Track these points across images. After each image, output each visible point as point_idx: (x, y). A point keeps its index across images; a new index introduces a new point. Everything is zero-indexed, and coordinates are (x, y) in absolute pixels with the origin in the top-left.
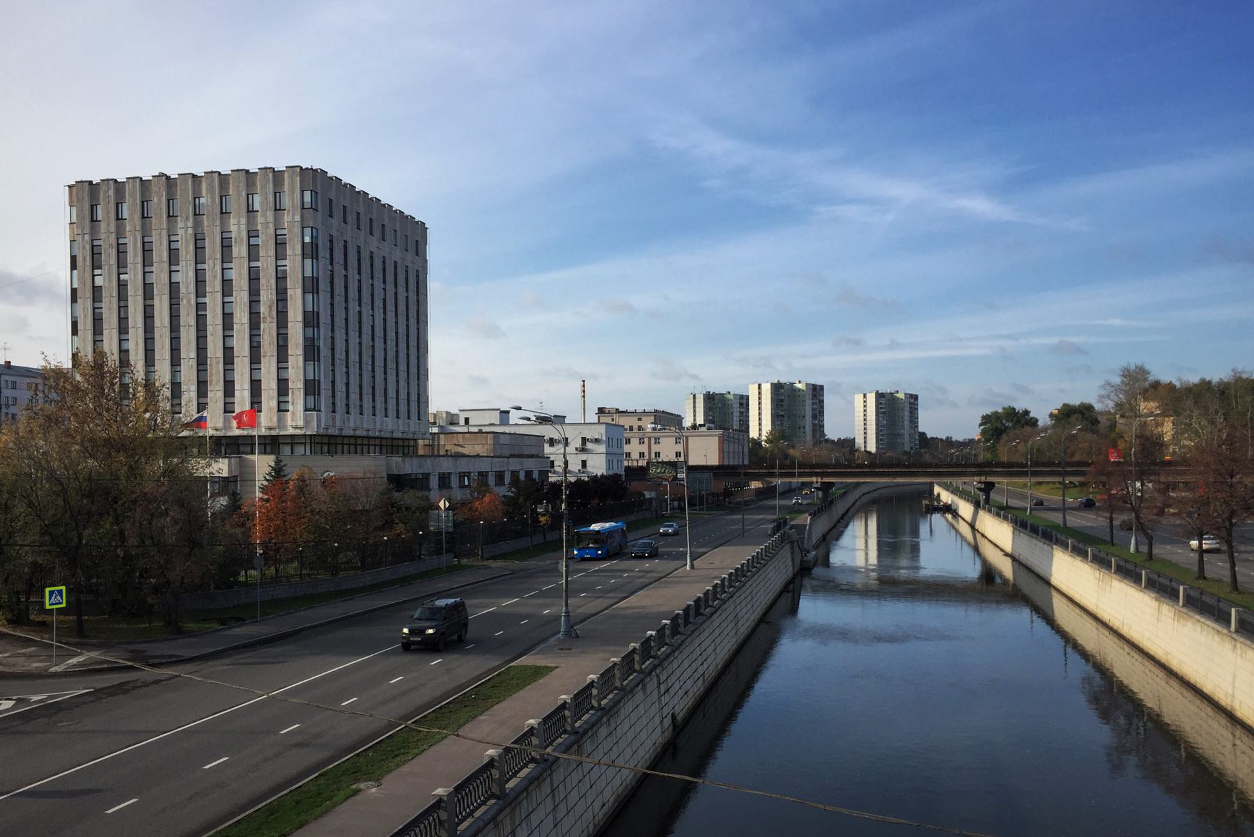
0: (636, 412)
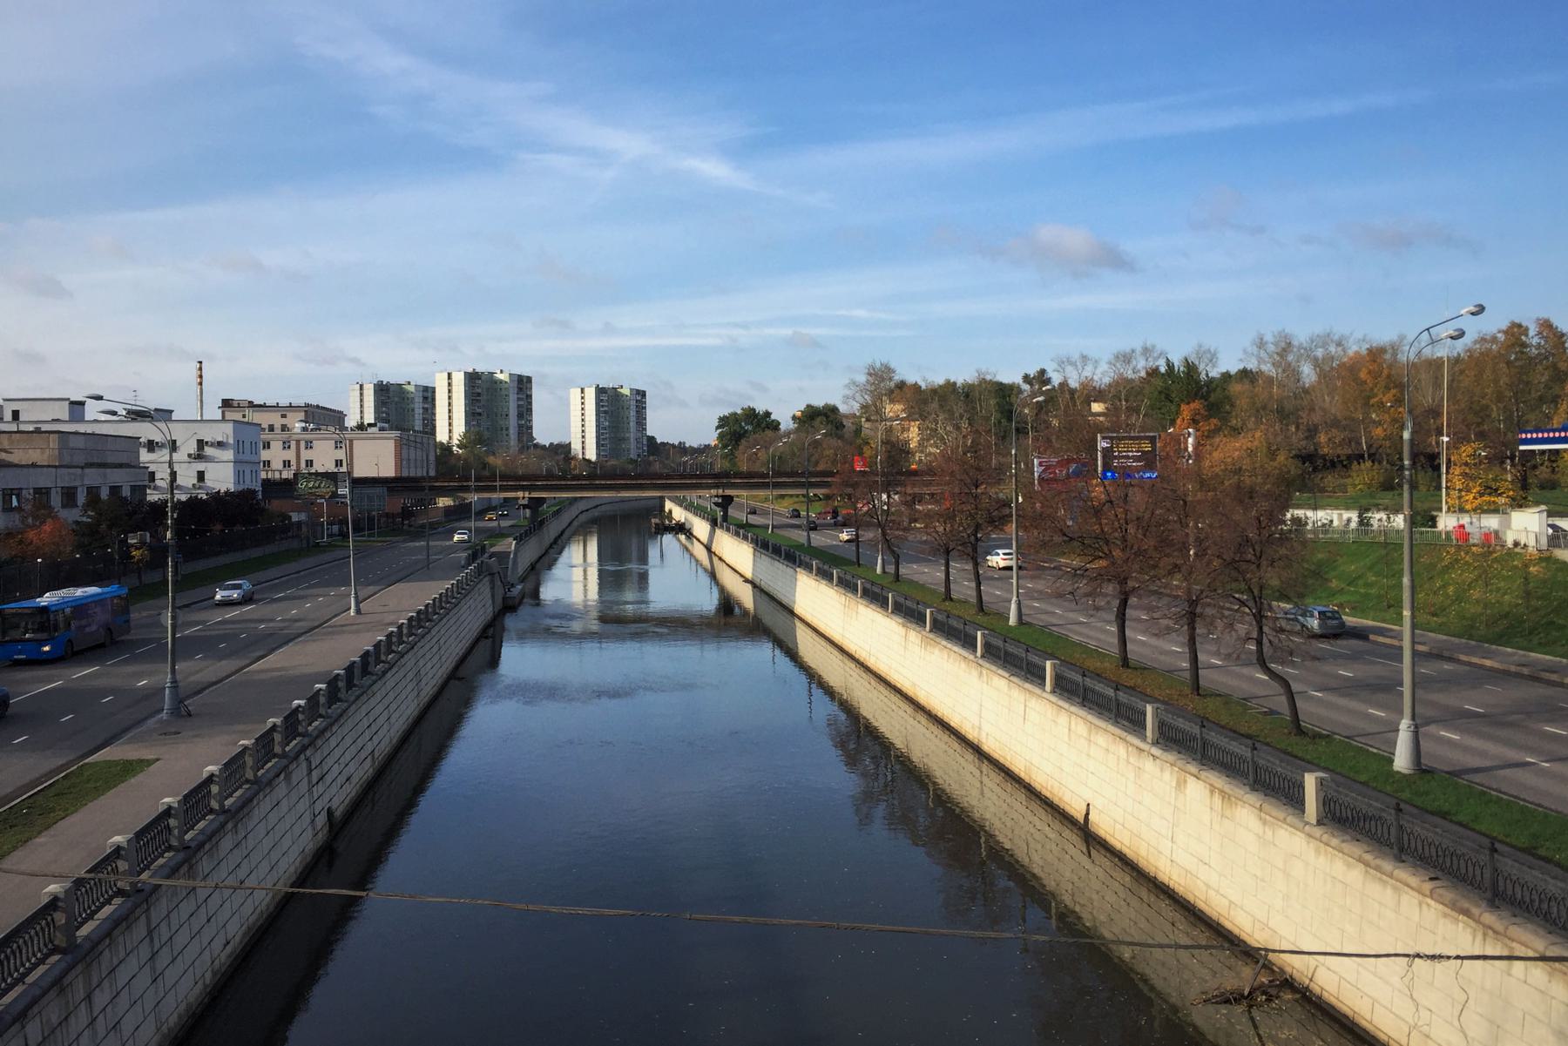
0: (291, 407)
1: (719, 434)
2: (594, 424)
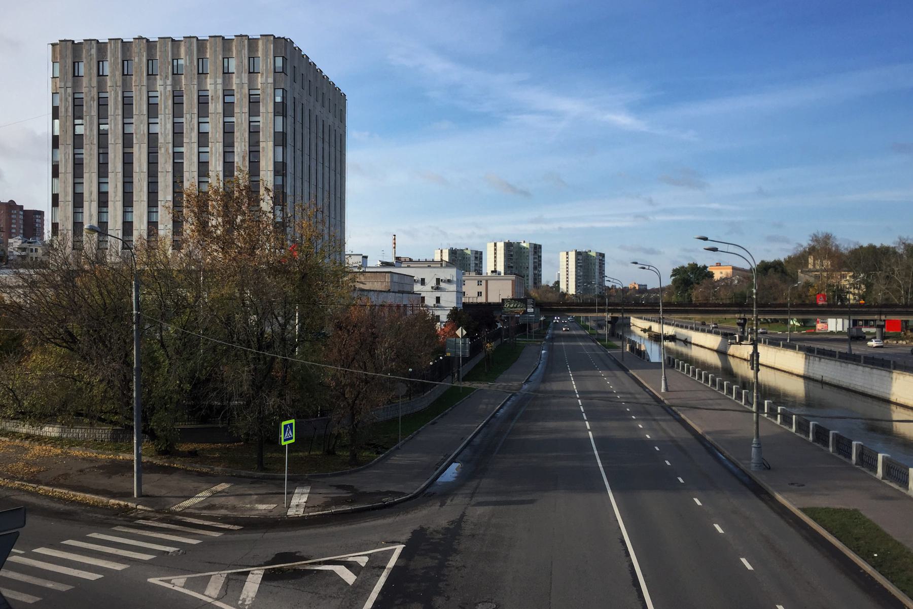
0: (433, 261)
1: (673, 280)
2: (574, 273)
